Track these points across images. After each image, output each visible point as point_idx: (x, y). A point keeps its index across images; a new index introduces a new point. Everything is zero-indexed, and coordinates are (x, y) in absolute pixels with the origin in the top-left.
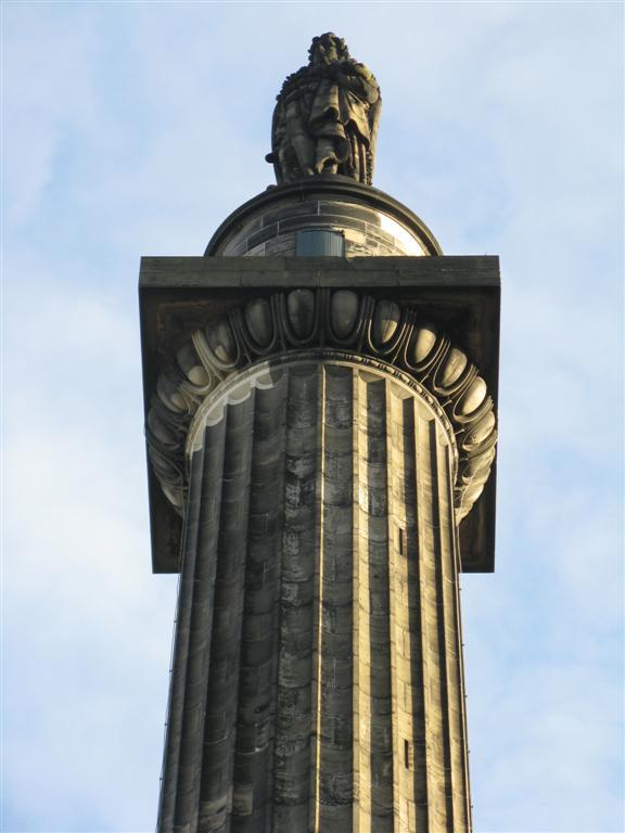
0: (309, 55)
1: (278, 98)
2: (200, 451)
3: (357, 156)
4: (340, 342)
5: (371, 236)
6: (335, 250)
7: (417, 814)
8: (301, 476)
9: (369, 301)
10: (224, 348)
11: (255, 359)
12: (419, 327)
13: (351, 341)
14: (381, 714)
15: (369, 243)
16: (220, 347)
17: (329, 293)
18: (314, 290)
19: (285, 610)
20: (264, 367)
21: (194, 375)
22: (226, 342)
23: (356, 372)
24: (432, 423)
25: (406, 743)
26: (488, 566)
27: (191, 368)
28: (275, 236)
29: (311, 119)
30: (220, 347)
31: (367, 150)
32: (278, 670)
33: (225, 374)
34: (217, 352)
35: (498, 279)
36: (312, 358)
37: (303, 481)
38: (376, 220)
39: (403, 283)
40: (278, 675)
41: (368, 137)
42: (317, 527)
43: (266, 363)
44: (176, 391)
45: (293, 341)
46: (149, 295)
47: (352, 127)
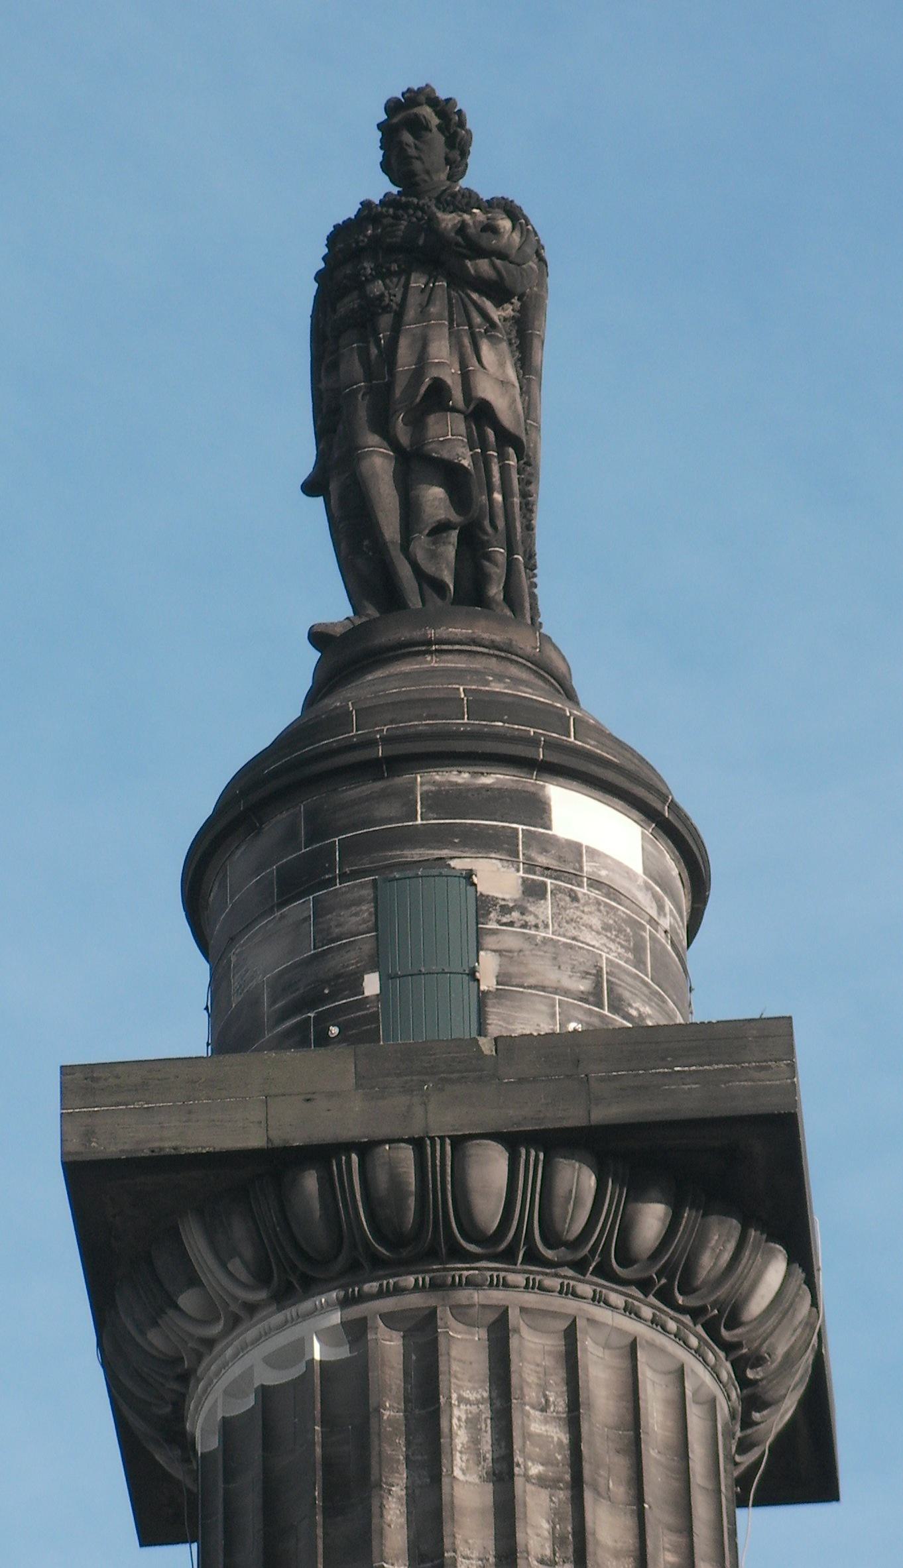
1: (319, 277)
7: (803, 1393)
9: (532, 1156)
10: (244, 1262)
11: (309, 1285)
12: (638, 1192)
15: (534, 891)
16: (237, 1261)
21: (188, 1300)
22: (248, 1252)
24: (680, 1374)
27: (181, 1292)
30: (237, 1261)
33: (252, 1308)
34: (229, 1266)
35: (795, 1104)
38: (538, 810)
42: (537, 833)
44: (155, 1324)
47: (482, 413)
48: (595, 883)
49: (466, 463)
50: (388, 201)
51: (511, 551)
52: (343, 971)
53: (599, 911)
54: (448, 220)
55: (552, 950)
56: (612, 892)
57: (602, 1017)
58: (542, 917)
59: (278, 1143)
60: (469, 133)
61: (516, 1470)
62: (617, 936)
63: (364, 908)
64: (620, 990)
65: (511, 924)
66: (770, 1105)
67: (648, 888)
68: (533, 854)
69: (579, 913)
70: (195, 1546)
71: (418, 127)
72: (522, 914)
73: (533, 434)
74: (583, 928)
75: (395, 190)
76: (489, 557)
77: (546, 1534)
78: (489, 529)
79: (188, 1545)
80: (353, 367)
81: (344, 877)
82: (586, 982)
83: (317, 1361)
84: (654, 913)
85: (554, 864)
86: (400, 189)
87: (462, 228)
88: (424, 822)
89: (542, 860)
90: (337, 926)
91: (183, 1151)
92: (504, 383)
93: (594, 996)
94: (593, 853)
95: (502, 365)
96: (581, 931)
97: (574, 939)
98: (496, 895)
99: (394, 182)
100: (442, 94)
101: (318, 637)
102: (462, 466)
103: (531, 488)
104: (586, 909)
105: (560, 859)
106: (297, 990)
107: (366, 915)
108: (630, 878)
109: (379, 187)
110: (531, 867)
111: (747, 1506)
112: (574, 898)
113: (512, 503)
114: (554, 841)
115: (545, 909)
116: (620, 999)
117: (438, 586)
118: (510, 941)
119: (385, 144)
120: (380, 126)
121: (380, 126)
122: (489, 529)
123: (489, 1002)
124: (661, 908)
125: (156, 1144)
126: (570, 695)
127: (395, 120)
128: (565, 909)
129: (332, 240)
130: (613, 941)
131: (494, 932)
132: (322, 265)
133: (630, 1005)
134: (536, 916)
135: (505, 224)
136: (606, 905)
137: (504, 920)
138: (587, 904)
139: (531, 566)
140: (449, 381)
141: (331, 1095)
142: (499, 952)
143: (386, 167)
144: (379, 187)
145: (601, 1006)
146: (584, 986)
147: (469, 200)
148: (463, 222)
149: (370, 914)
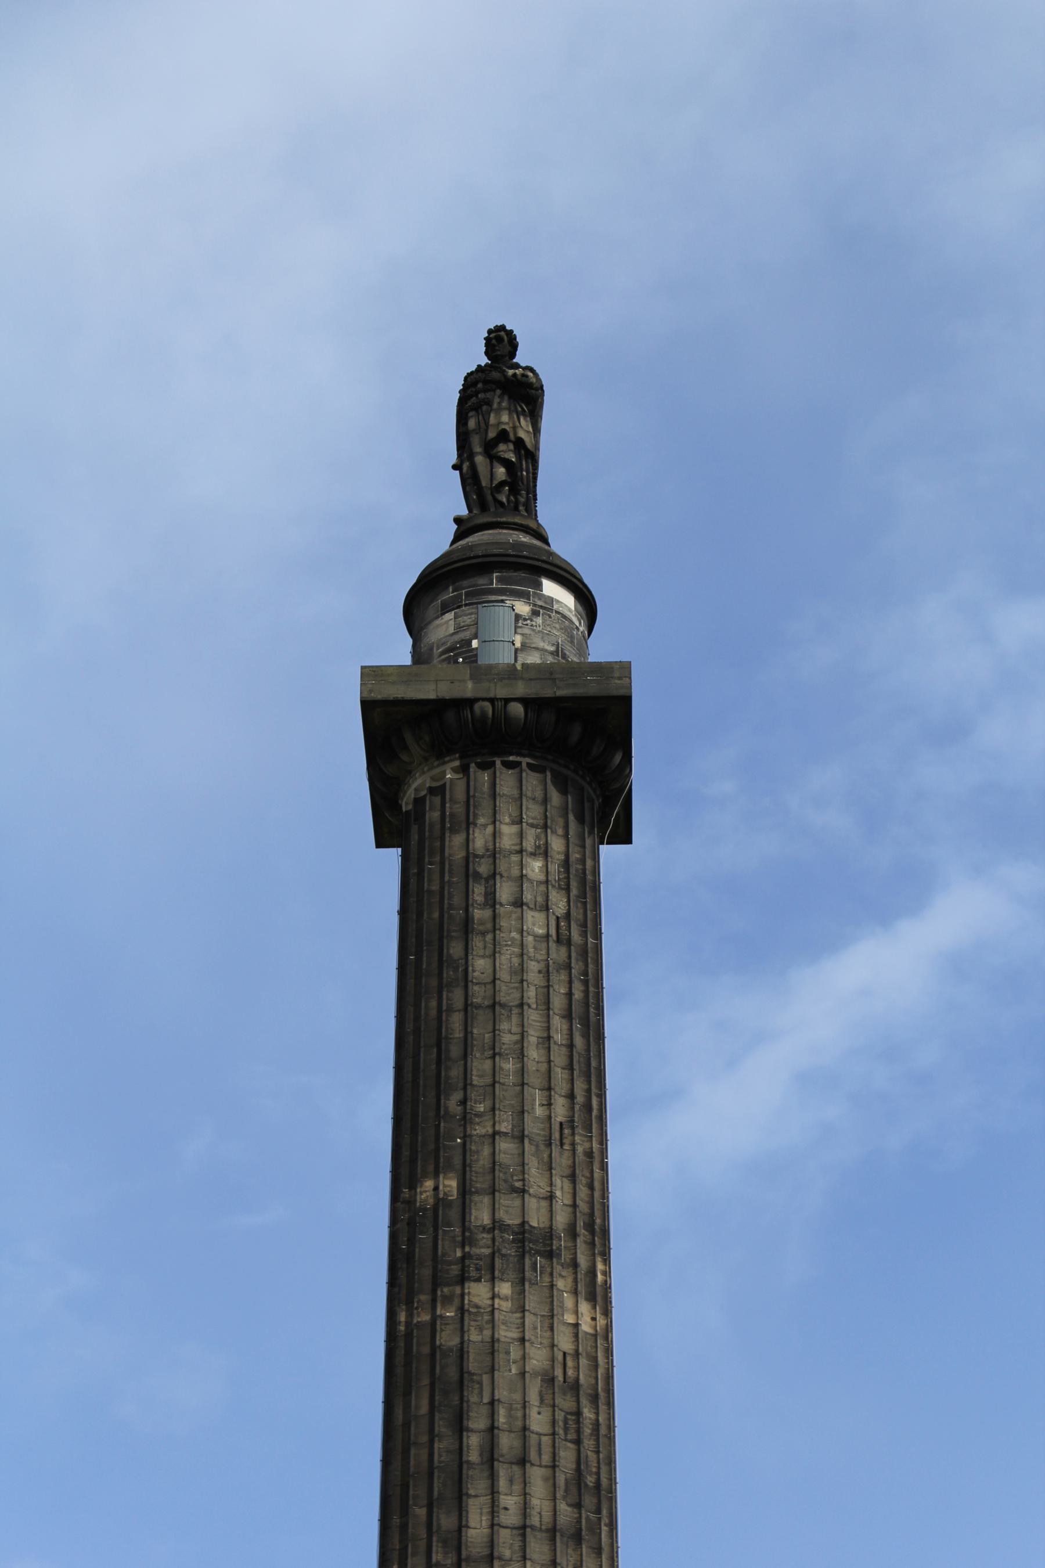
0: (485, 342)
2: (410, 810)
3: (525, 473)
5: (535, 605)
8: (485, 876)
14: (543, 1105)
15: (535, 613)
17: (503, 702)
18: (492, 701)
19: (475, 1011)
23: (524, 765)
25: (561, 1124)
26: (627, 839)
28: (459, 607)
32: (472, 1070)
35: (631, 693)
37: (487, 880)
38: (539, 586)
39: (560, 693)
40: (472, 1075)
43: (457, 755)
46: (368, 706)
47: (519, 443)
48: (557, 612)
49: (513, 460)
50: (487, 365)
51: (528, 494)
54: (511, 372)
55: (541, 635)
56: (565, 617)
57: (558, 660)
58: (538, 623)
59: (440, 697)
60: (518, 343)
61: (523, 820)
63: (473, 616)
64: (565, 651)
65: (527, 625)
66: (622, 692)
67: (576, 616)
68: (536, 600)
70: (400, 850)
71: (499, 339)
72: (531, 621)
73: (537, 452)
75: (490, 362)
76: (520, 495)
77: (533, 844)
78: (521, 484)
79: (396, 849)
80: (472, 424)
81: (466, 605)
83: (461, 762)
84: (578, 625)
85: (543, 605)
87: (515, 375)
89: (540, 603)
91: (406, 699)
92: (528, 432)
93: (555, 653)
94: (558, 602)
95: (527, 426)
97: (549, 631)
99: (489, 359)
100: (508, 328)
101: (458, 520)
102: (512, 461)
103: (536, 471)
105: (546, 603)
107: (474, 619)
108: (570, 611)
109: (484, 361)
110: (535, 605)
111: (604, 844)
112: (550, 617)
113: (530, 476)
114: (544, 595)
115: (539, 620)
116: (565, 654)
117: (502, 504)
118: (526, 631)
119: (486, 345)
120: (485, 339)
121: (485, 339)
122: (521, 484)
123: (519, 652)
124: (580, 624)
125: (395, 696)
127: (491, 336)
128: (546, 620)
129: (466, 379)
130: (563, 633)
131: (521, 627)
132: (462, 387)
133: (569, 657)
134: (536, 623)
135: (531, 374)
136: (561, 620)
137: (525, 623)
138: (554, 619)
139: (535, 499)
140: (508, 429)
141: (460, 681)
142: (522, 635)
143: (487, 353)
144: (484, 361)
145: (558, 656)
146: (552, 649)
147: (517, 366)
148: (515, 373)
149: (475, 618)
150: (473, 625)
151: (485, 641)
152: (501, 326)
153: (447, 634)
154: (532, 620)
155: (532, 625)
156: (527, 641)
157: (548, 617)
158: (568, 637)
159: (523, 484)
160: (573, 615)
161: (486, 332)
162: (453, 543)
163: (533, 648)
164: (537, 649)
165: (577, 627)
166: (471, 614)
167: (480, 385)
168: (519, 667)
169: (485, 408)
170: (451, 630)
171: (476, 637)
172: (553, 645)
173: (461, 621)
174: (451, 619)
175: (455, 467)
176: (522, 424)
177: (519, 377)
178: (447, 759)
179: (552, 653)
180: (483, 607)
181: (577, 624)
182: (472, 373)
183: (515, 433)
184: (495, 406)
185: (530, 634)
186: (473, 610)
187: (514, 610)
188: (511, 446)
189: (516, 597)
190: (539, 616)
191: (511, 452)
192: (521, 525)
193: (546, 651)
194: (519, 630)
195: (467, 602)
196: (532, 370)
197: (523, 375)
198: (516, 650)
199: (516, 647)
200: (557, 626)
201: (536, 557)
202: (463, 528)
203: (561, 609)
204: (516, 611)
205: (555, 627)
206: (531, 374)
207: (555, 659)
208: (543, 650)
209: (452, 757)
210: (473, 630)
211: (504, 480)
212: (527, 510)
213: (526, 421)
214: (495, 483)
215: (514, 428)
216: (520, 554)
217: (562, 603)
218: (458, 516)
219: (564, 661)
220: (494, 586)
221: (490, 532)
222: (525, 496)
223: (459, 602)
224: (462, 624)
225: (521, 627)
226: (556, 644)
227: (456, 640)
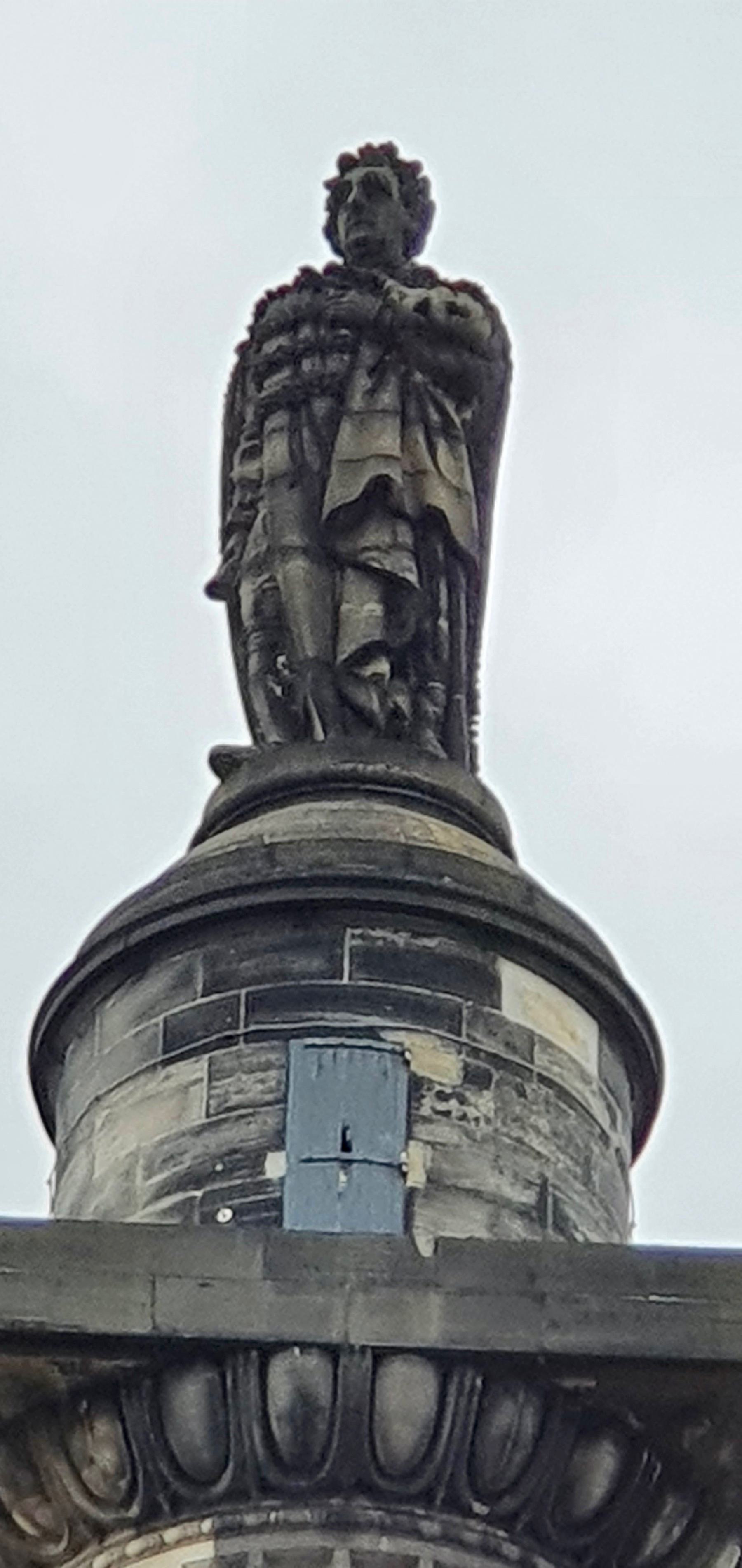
1: (242, 349)
3: (443, 624)
4: (394, 1487)
5: (475, 1052)
6: (341, 211)
13: (418, 1486)
20: (199, 1537)
28: (230, 1041)
29: (342, 657)
31: (463, 809)
36: (326, 1527)
41: (473, 552)
43: (207, 1525)
45: (273, 1476)
48: (543, 1080)
50: (330, 269)
51: (450, 692)
52: (241, 1145)
53: (548, 1112)
54: (413, 296)
59: (165, 1330)
62: (567, 1146)
69: (526, 1112)
72: (462, 1103)
74: (530, 1130)
75: (339, 261)
78: (429, 659)
81: (249, 1037)
82: (528, 1192)
86: (339, 261)
88: (352, 983)
89: (490, 1045)
90: (237, 1093)
96: (527, 1133)
98: (434, 1078)
99: (337, 250)
100: (405, 154)
104: (535, 1108)
106: (181, 1163)
107: (273, 1083)
112: (522, 1094)
114: (503, 1022)
116: (566, 1219)
118: (444, 1132)
120: (328, 185)
121: (328, 185)
123: (418, 1201)
126: (508, 851)
127: (348, 176)
129: (261, 309)
135: (476, 308)
139: (473, 710)
142: (433, 1144)
143: (330, 231)
146: (529, 1197)
147: (428, 278)
149: (279, 1083)
150: (269, 1104)
151: (310, 1160)
152: (382, 147)
153: (185, 1126)
154: (462, 1101)
155: (464, 1117)
156: (445, 1166)
157: (514, 1094)
158: (577, 1163)
159: (436, 657)
160: (593, 1092)
161: (362, 144)
162: (200, 838)
163: (468, 1191)
164: (476, 1194)
165: (603, 1131)
166: (267, 1067)
167: (306, 332)
168: (426, 1249)
169: (321, 406)
170: (197, 1116)
171: (278, 1142)
172: (529, 1184)
173: (232, 1089)
174: (200, 1080)
175: (213, 590)
176: (441, 465)
177: (440, 315)
178: (171, 1535)
179: (523, 1212)
180: (308, 1046)
181: (604, 1120)
182: (283, 291)
183: (418, 492)
184: (357, 402)
185: (457, 1146)
186: (273, 1057)
187: (407, 1063)
188: (405, 536)
189: (416, 1019)
190: (487, 1088)
191: (405, 553)
192: (433, 791)
193: (507, 1204)
194: (420, 1130)
195: (252, 1028)
196: (475, 292)
197: (452, 309)
198: (411, 1195)
199: (410, 1183)
200: (543, 1124)
201: (480, 893)
202: (241, 784)
203: (556, 1069)
204: (413, 1067)
205: (538, 1131)
206: (476, 308)
207: (534, 1232)
208: (497, 1202)
209: (191, 1528)
210: (269, 1120)
211: (378, 642)
212: (445, 742)
213: (457, 459)
214: (347, 648)
215: (416, 475)
216: (434, 882)
217: (561, 1051)
218: (224, 747)
219: (561, 1239)
220: (345, 981)
221: (335, 805)
222: (441, 698)
223: (230, 1027)
224: (235, 1099)
225: (426, 1120)
226: (538, 1181)
227: (213, 1149)
